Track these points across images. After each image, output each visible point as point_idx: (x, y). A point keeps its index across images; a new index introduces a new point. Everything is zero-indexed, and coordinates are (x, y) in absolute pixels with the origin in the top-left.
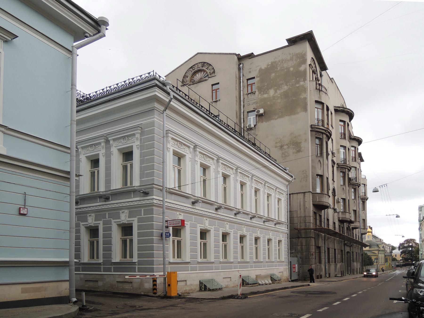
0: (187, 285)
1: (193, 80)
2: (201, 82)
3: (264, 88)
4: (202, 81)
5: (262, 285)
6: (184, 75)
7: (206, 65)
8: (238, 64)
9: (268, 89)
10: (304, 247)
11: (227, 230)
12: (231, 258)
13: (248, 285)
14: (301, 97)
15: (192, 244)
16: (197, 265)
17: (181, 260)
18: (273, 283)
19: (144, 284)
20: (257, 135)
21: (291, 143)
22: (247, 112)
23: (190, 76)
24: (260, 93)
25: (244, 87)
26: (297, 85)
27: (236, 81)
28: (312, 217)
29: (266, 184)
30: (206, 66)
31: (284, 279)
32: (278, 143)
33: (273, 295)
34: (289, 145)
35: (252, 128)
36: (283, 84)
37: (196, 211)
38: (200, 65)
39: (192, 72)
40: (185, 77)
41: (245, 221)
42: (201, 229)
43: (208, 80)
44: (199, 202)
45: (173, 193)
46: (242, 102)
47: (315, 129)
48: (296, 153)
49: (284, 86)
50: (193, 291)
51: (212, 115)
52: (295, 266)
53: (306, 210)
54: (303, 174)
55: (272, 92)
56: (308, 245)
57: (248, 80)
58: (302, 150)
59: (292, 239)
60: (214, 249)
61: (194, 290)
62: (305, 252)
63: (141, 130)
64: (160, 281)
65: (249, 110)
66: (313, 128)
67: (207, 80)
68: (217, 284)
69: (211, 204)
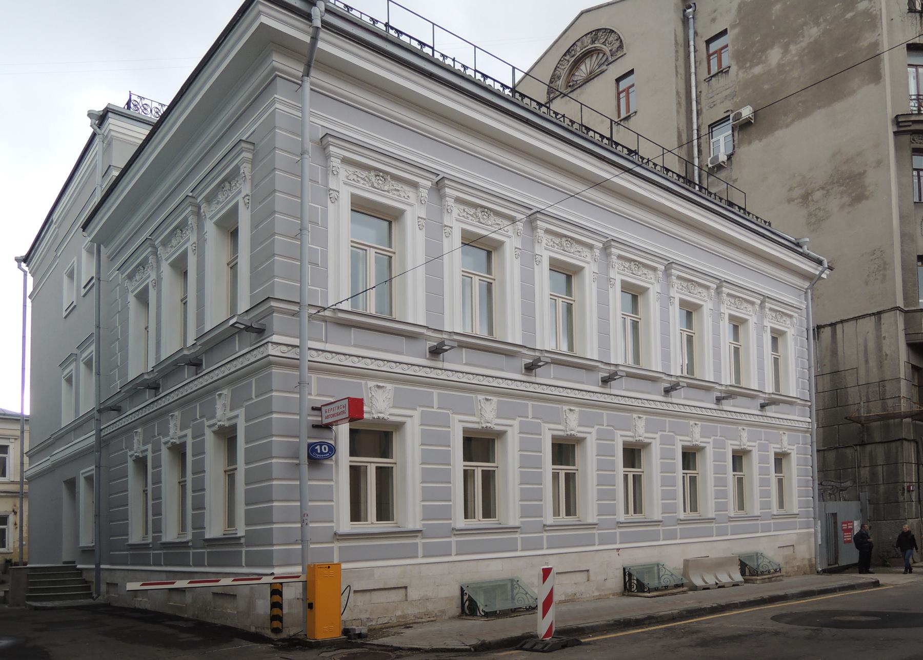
0: (409, 599)
1: (574, 81)
2: (591, 80)
3: (754, 49)
4: (593, 78)
5: (704, 589)
6: (552, 76)
7: (602, 35)
8: (681, 7)
9: (764, 50)
10: (880, 469)
11: (745, 445)
12: (754, 506)
13: (755, 575)
14: (861, 44)
15: (665, 482)
16: (676, 526)
17: (641, 517)
18: (746, 581)
19: (257, 600)
20: (735, 180)
21: (836, 180)
22: (709, 126)
23: (566, 74)
24: (741, 68)
25: (698, 64)
26: (849, 15)
27: (677, 52)
28: (903, 383)
29: (724, 289)
30: (602, 37)
31: (798, 567)
32: (796, 189)
33: (691, 632)
34: (829, 187)
35: (722, 164)
36: (805, 24)
37: (539, 389)
38: (587, 40)
39: (570, 63)
40: (554, 78)
41: (640, 401)
42: (684, 448)
43: (606, 70)
44: (541, 361)
45: (350, 324)
46: (694, 103)
47: (910, 126)
48: (849, 205)
49: (811, 28)
50: (432, 619)
51: (522, 100)
52: (853, 525)
53: (886, 362)
54: (872, 260)
55: (775, 55)
56: (893, 464)
57: (709, 42)
58: (867, 193)
59: (844, 449)
60: (662, 490)
61: (436, 616)
62: (884, 484)
63: (253, 150)
64: (291, 593)
65: (712, 120)
66: (901, 124)
67: (604, 72)
68: (525, 592)
69: (586, 367)
